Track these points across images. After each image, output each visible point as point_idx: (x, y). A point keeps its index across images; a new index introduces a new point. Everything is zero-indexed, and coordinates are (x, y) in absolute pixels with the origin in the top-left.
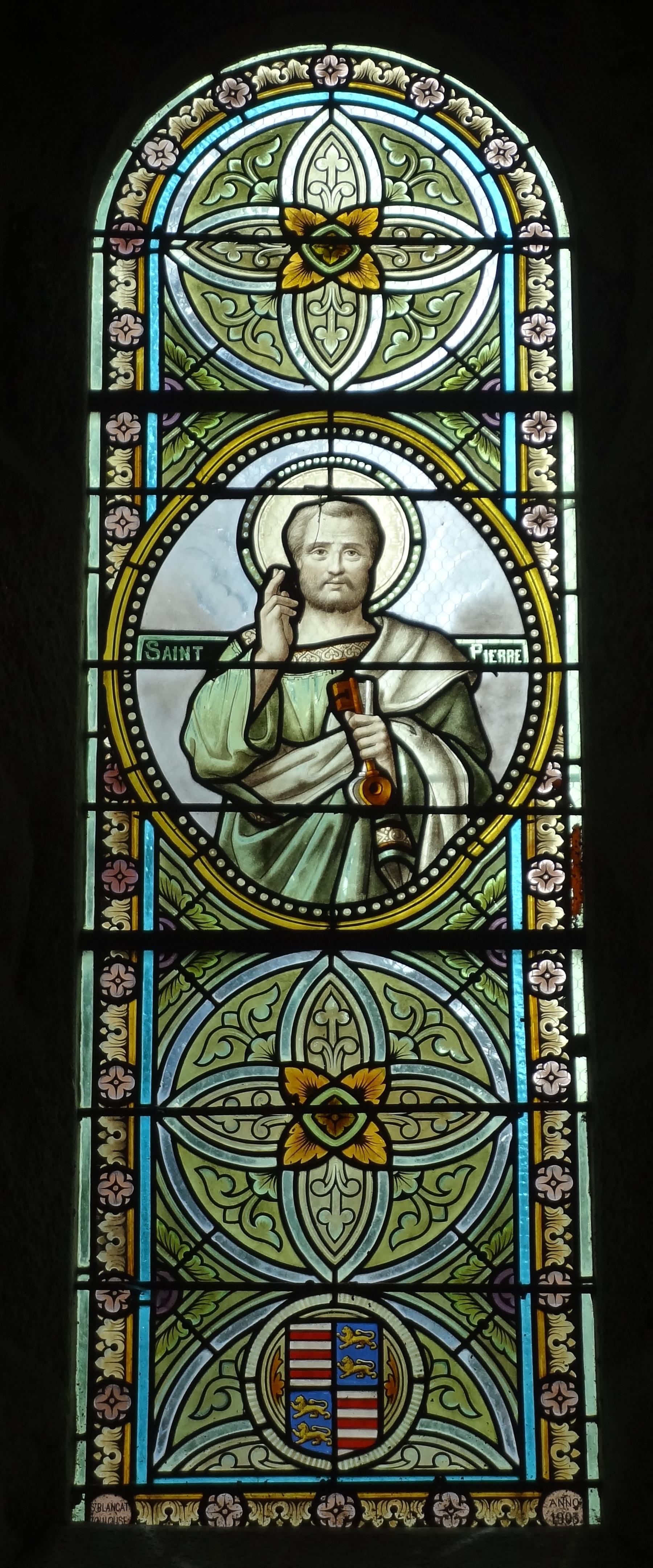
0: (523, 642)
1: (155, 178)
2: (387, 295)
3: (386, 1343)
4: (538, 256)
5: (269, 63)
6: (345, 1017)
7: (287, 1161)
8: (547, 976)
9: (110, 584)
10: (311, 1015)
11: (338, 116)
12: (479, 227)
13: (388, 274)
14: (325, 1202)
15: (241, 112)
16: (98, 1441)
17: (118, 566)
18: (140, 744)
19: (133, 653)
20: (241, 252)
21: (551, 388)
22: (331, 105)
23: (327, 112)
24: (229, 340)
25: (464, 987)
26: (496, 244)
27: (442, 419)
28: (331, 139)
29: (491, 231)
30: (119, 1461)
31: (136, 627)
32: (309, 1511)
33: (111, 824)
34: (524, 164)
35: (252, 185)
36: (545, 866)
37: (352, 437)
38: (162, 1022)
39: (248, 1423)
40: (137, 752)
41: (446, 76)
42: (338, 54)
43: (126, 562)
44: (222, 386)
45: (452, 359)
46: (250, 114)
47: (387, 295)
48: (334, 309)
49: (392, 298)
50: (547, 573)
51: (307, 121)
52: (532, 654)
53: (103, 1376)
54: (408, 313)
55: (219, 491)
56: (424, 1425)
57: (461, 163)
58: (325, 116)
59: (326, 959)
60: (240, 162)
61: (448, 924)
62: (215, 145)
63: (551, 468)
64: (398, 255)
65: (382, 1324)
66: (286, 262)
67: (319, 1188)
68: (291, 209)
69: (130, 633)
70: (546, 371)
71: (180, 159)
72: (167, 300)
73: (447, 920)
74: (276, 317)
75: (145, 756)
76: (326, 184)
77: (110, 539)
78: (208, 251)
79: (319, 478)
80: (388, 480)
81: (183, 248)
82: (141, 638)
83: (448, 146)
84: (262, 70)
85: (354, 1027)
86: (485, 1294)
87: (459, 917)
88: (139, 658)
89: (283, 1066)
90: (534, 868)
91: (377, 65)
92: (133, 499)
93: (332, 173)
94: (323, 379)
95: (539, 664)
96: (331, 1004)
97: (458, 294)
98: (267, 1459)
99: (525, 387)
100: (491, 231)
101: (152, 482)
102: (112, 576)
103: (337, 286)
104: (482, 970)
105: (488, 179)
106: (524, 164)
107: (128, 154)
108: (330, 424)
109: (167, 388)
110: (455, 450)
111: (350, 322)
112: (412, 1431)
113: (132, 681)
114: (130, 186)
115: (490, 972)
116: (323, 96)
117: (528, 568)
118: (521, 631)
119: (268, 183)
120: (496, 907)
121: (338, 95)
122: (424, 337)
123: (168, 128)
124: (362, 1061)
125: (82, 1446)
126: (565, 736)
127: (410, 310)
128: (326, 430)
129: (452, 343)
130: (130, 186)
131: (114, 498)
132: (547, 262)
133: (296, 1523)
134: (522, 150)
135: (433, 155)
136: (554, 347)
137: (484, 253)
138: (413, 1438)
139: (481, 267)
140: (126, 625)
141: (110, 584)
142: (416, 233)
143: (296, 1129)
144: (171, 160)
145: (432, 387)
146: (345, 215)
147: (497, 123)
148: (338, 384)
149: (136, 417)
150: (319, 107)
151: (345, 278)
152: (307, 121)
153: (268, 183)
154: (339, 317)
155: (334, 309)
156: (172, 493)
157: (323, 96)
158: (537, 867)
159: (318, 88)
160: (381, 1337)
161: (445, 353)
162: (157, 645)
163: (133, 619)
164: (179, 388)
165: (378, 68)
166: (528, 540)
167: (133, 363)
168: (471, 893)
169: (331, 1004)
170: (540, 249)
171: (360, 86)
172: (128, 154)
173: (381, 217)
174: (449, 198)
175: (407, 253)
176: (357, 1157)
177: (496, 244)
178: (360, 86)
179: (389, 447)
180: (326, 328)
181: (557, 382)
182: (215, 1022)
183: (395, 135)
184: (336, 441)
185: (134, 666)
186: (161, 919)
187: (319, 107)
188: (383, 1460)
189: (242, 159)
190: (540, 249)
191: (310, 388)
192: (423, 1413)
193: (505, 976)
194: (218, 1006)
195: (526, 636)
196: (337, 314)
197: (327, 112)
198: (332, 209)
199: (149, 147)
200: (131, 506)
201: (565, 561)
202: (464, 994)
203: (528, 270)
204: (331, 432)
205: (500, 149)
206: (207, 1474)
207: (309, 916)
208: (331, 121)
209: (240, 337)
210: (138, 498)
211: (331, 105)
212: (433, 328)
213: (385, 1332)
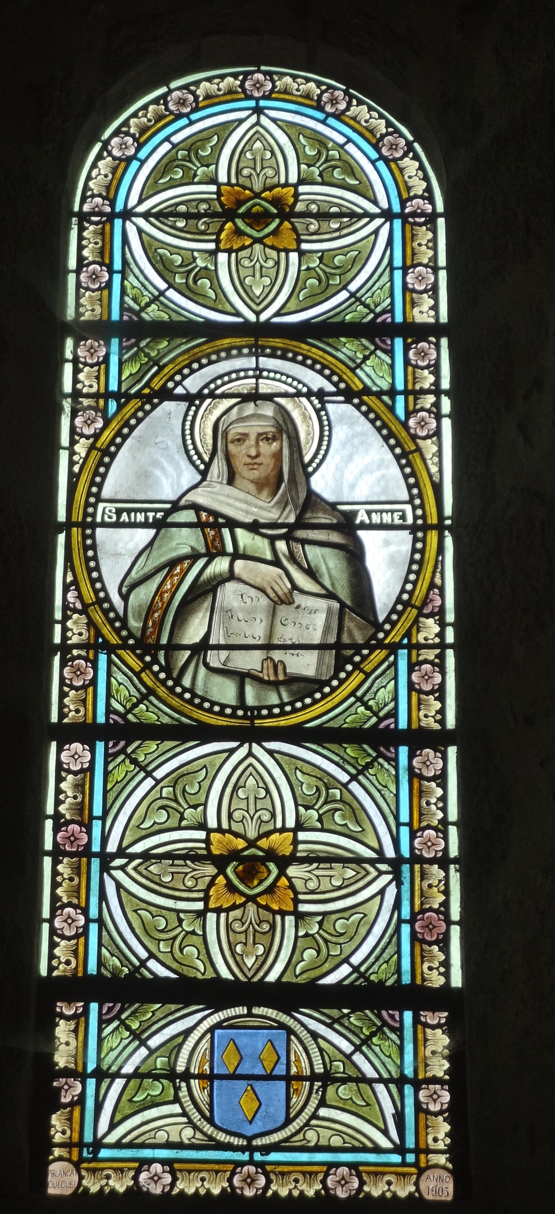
0: (408, 508)
1: (119, 165)
2: (300, 917)
3: (293, 1046)
4: (420, 225)
5: (209, 80)
6: (263, 793)
7: (212, 905)
8: (431, 927)
9: (76, 469)
10: (235, 788)
11: (264, 120)
12: (375, 202)
13: (303, 237)
14: (242, 938)
15: (187, 115)
16: (69, 624)
17: (83, 455)
18: (98, 585)
19: (94, 515)
20: (172, 873)
21: (437, 727)
22: (258, 111)
23: (255, 116)
24: (160, 951)
25: (360, 772)
26: (388, 215)
27: (346, 748)
28: (258, 301)
29: (390, 853)
30: (77, 883)
31: (98, 496)
32: (228, 1181)
33: (69, 708)
34: (411, 155)
35: (182, 810)
36: (431, 917)
37: (273, 356)
38: (111, 797)
39: (177, 1105)
40: (96, 592)
41: (351, 91)
42: (265, 73)
43: (92, 447)
44: (169, 318)
45: (353, 300)
46: (194, 117)
47: (300, 917)
48: (260, 263)
49: (303, 824)
50: (429, 462)
51: (241, 121)
52: (415, 518)
53: (65, 818)
54: (318, 933)
55: (166, 395)
56: (323, 1112)
57: (360, 154)
58: (254, 119)
59: (246, 745)
60: (171, 789)
61: (345, 723)
62: (167, 139)
63: (437, 712)
64: (310, 879)
65: (290, 1031)
66: (212, 884)
67: (246, 263)
68: (226, 187)
69: (92, 500)
70: (433, 713)
71: (138, 150)
72: (128, 255)
73: (345, 720)
74: (201, 933)
75: (102, 595)
76: (247, 811)
77: (79, 435)
78: (145, 872)
79: (245, 385)
80: (300, 386)
81: (122, 868)
82: (101, 506)
83: (349, 140)
84: (205, 85)
85: (275, 161)
86: (376, 1011)
87: (357, 716)
88: (99, 519)
89: (209, 831)
90: (420, 837)
91: (294, 81)
92: (87, 653)
93: (258, 275)
94: (251, 312)
95: (422, 525)
96: (251, 781)
97: (357, 252)
98: (194, 1137)
99: (414, 726)
100: (385, 205)
101: (91, 1067)
102: (78, 463)
103: (255, 906)
104: (375, 759)
105: (381, 164)
106: (411, 155)
107: (98, 146)
108: (256, 346)
109: (125, 318)
110: (356, 368)
111: (273, 272)
112: (314, 1116)
113: (93, 536)
114: (99, 170)
115: (381, 760)
116: (252, 103)
117: (412, 452)
118: (405, 497)
119: (196, 810)
120: (387, 709)
121: (262, 103)
122: (331, 282)
123: (129, 127)
124: (275, 827)
125: (46, 927)
126: (443, 562)
127: (319, 929)
128: (254, 350)
129: (353, 287)
130: (99, 170)
131: (71, 653)
132: (436, 699)
133: (216, 1191)
134: (409, 144)
135: (341, 787)
136: (440, 692)
137: (378, 221)
138: (314, 1122)
139: (376, 232)
140: (89, 494)
141: (76, 469)
142: (325, 208)
143: (221, 880)
144: (132, 151)
145: (337, 319)
146: (268, 193)
147: (389, 124)
148: (263, 317)
149: (86, 747)
150: (250, 112)
151: (262, 901)
152: (241, 121)
153: (196, 810)
154: (264, 269)
155: (260, 263)
156: (129, 397)
157: (252, 103)
158: (421, 836)
159: (249, 97)
160: (289, 1041)
161: (348, 295)
162: (114, 510)
163: (94, 490)
164: (136, 319)
165: (295, 84)
166: (414, 437)
167: (70, 1119)
168: (366, 699)
169: (251, 781)
170: (423, 219)
171: (282, 96)
172: (98, 146)
173: (296, 195)
174: (356, 827)
175: (317, 877)
176: (275, 244)
177: (388, 215)
178: (282, 96)
179: (303, 363)
180: (254, 276)
181: (437, 316)
182: (155, 794)
183: (307, 768)
184: (261, 359)
185: (94, 525)
186: (111, 716)
187: (250, 112)
188: (287, 1140)
189: (174, 787)
190: (423, 219)
191: (240, 320)
192: (323, 1103)
193: (393, 763)
194: (158, 782)
195: (411, 501)
196: (255, 931)
197: (255, 116)
198: (258, 247)
199: (115, 141)
200: (86, 659)
201: (442, 456)
202: (361, 778)
203: (413, 236)
204: (257, 351)
205: (392, 145)
206: (143, 1146)
207: (233, 715)
208: (258, 123)
209: (170, 950)
210: (101, 402)
211: (258, 111)
212: (338, 277)
213: (292, 1037)
